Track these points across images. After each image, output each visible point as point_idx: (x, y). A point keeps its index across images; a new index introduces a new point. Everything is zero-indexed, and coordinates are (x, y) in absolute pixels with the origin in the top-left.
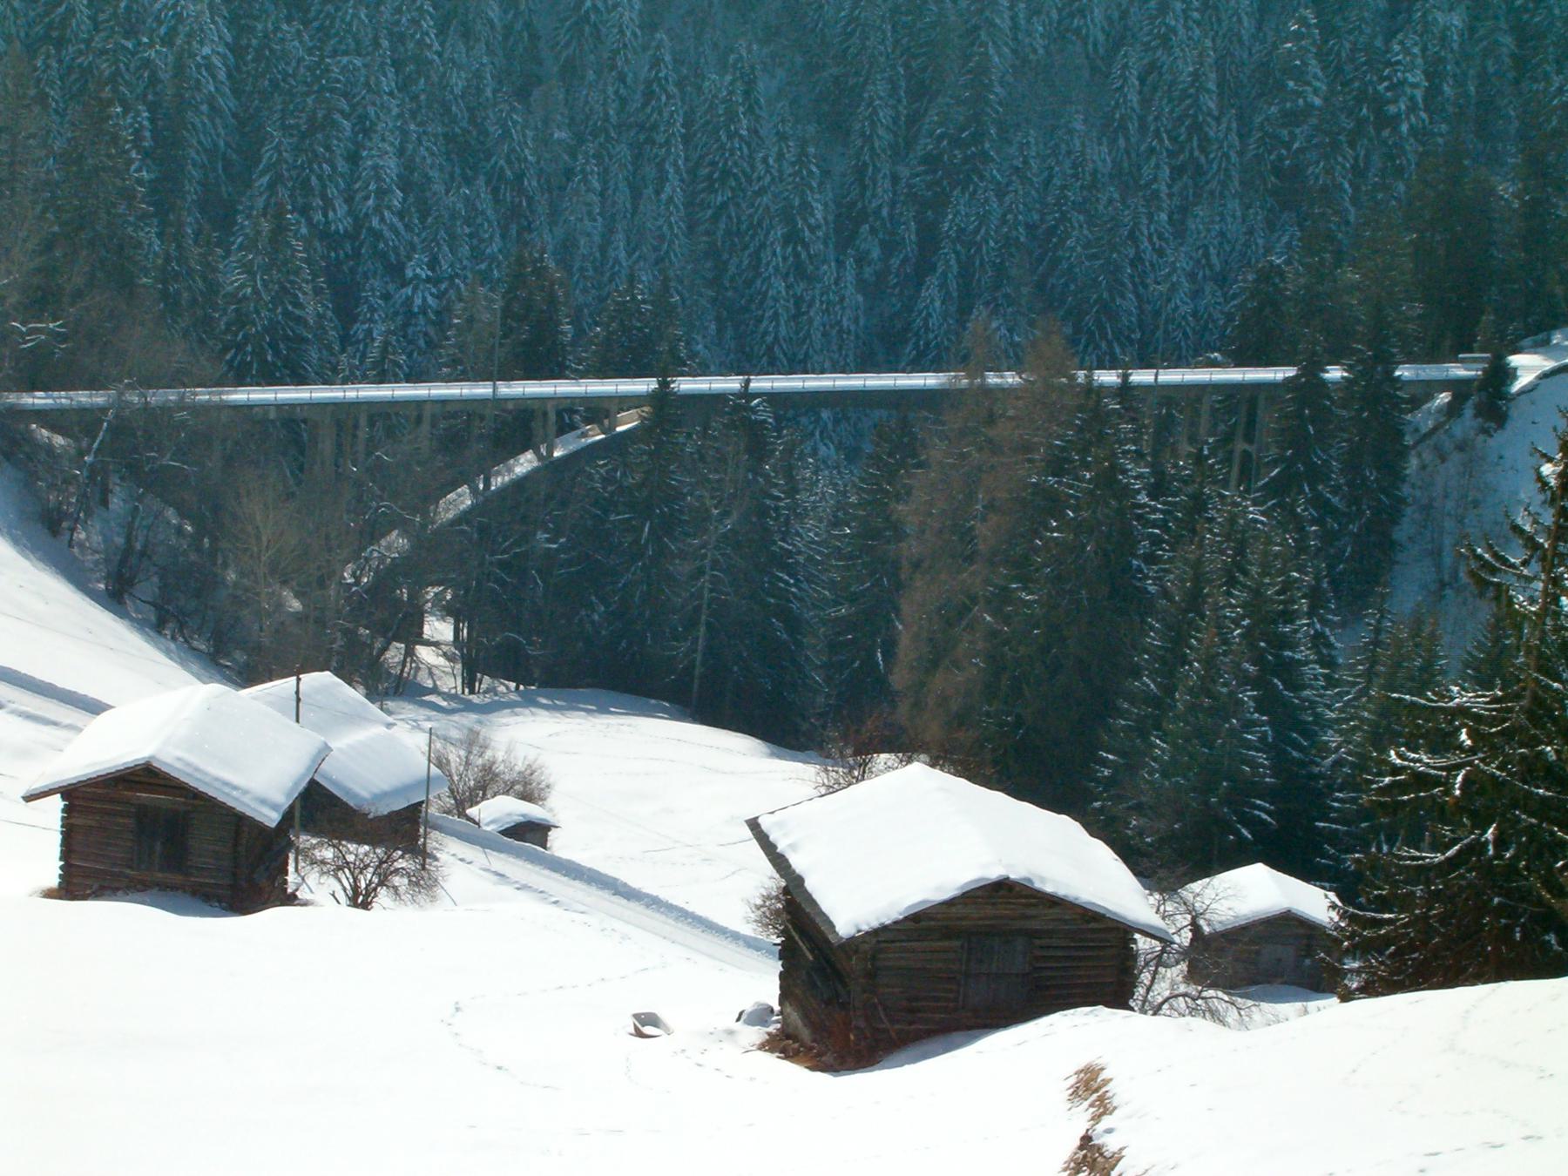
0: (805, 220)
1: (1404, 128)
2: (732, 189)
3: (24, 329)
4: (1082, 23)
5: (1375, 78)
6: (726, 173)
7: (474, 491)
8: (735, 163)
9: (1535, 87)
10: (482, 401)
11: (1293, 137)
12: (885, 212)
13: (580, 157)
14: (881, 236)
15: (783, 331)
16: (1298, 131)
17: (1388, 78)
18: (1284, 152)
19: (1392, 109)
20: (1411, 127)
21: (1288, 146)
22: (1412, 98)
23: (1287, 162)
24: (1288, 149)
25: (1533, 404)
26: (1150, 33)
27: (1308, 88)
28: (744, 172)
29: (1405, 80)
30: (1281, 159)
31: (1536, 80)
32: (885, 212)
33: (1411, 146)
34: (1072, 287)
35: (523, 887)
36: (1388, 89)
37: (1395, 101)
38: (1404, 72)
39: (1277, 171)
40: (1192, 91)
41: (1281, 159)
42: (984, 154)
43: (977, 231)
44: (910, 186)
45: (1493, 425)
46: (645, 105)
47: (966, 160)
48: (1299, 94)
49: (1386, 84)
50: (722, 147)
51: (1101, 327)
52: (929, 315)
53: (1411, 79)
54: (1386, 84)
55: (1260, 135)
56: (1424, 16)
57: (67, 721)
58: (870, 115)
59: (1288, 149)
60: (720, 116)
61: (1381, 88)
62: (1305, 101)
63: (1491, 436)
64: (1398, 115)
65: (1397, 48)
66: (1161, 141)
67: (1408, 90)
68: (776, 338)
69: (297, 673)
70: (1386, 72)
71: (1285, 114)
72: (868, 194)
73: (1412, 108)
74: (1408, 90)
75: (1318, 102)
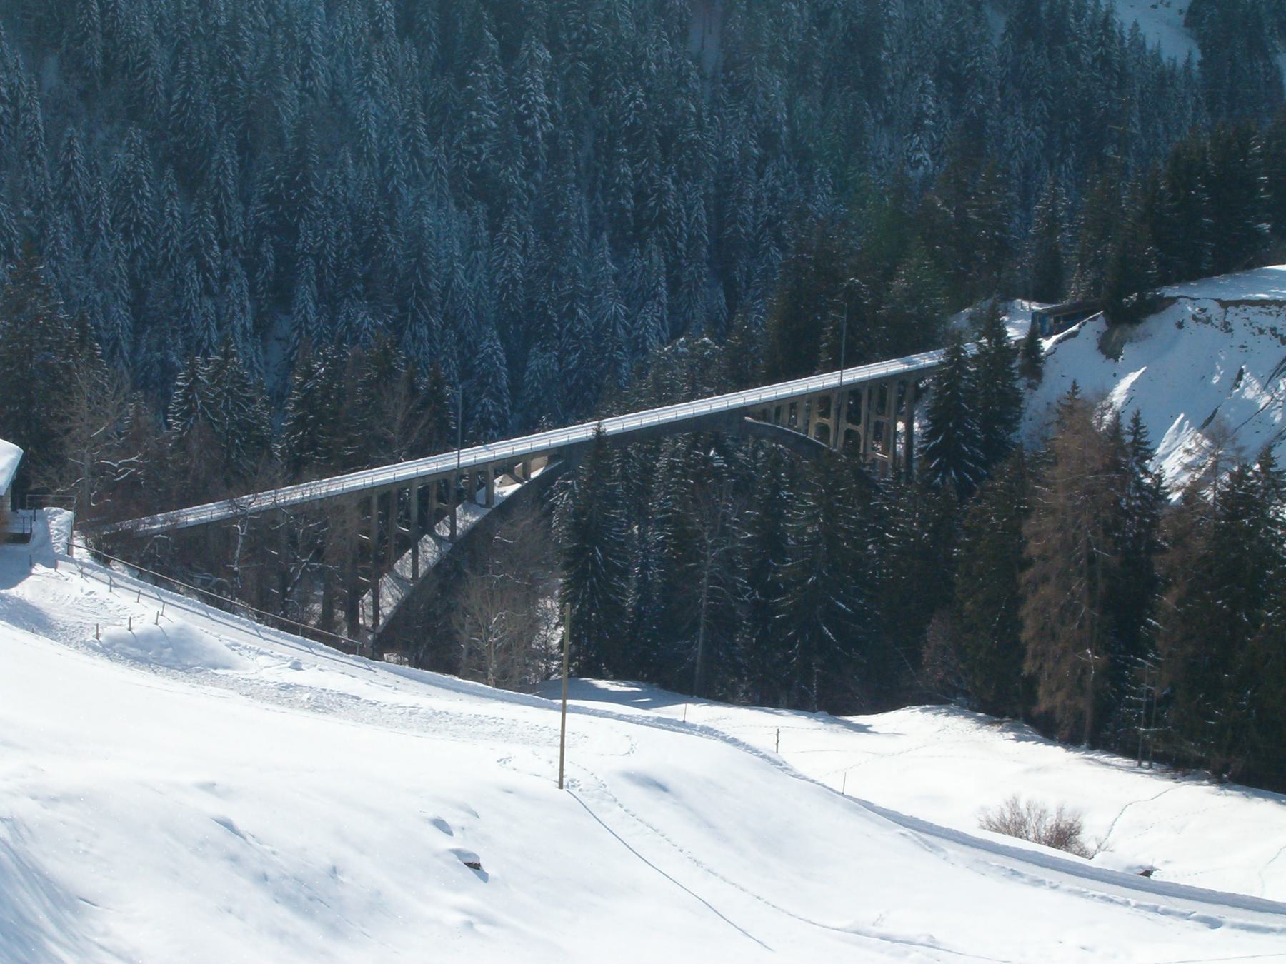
0: (209, 254)
1: (539, 135)
2: (144, 236)
3: (116, 465)
4: (312, 83)
6: (139, 225)
8: (145, 218)
10: (450, 472)
11: (480, 151)
12: (241, 239)
13: (51, 227)
14: (240, 256)
15: (214, 337)
17: (525, 101)
18: (475, 162)
19: (529, 122)
21: (477, 158)
23: (478, 169)
24: (478, 159)
25: (1057, 362)
26: (362, 85)
28: (150, 223)
29: (536, 101)
30: (473, 166)
31: (609, 91)
32: (241, 239)
33: (543, 147)
34: (396, 280)
35: (1166, 913)
36: (525, 109)
37: (530, 116)
38: (534, 96)
39: (472, 176)
41: (473, 166)
42: (311, 190)
43: (323, 246)
45: (1034, 381)
46: (65, 181)
48: (478, 120)
49: (523, 106)
50: (134, 206)
51: (419, 305)
52: (307, 312)
53: (540, 100)
54: (523, 106)
57: (1121, 899)
58: (223, 170)
60: (130, 184)
61: (521, 108)
62: (486, 125)
63: (1036, 389)
64: (534, 127)
65: (528, 79)
67: (538, 108)
68: (210, 342)
72: (226, 227)
73: (543, 121)
74: (538, 108)
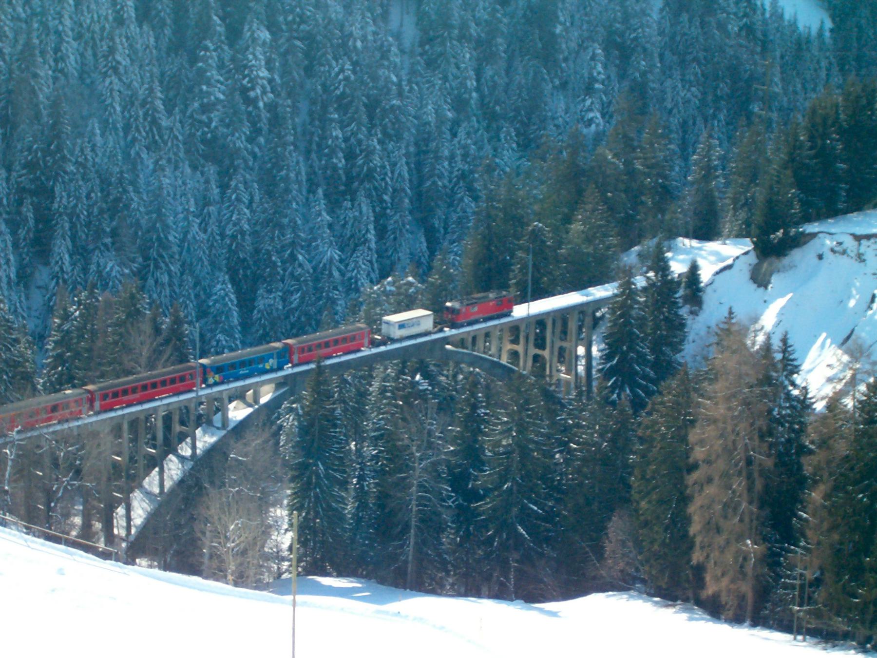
1: (261, 104)
5: (241, 77)
7: (182, 459)
9: (322, 69)
11: (210, 120)
16: (212, 115)
17: (248, 75)
18: (206, 129)
19: (252, 94)
20: (265, 104)
21: (208, 125)
22: (263, 87)
24: (209, 127)
26: (105, 66)
27: (217, 89)
30: (204, 134)
39: (204, 141)
40: (149, 99)
44: (18, 183)
47: (55, 162)
51: (162, 256)
52: (63, 263)
54: (247, 79)
55: (190, 121)
56: (252, 35)
59: (209, 127)
64: (257, 98)
65: (251, 57)
66: (140, 132)
69: (295, 594)
70: (246, 72)
71: (202, 105)
73: (264, 92)
74: (260, 81)
75: (222, 97)
